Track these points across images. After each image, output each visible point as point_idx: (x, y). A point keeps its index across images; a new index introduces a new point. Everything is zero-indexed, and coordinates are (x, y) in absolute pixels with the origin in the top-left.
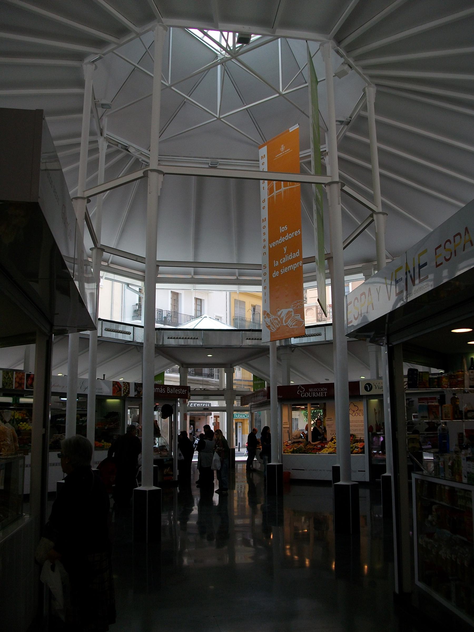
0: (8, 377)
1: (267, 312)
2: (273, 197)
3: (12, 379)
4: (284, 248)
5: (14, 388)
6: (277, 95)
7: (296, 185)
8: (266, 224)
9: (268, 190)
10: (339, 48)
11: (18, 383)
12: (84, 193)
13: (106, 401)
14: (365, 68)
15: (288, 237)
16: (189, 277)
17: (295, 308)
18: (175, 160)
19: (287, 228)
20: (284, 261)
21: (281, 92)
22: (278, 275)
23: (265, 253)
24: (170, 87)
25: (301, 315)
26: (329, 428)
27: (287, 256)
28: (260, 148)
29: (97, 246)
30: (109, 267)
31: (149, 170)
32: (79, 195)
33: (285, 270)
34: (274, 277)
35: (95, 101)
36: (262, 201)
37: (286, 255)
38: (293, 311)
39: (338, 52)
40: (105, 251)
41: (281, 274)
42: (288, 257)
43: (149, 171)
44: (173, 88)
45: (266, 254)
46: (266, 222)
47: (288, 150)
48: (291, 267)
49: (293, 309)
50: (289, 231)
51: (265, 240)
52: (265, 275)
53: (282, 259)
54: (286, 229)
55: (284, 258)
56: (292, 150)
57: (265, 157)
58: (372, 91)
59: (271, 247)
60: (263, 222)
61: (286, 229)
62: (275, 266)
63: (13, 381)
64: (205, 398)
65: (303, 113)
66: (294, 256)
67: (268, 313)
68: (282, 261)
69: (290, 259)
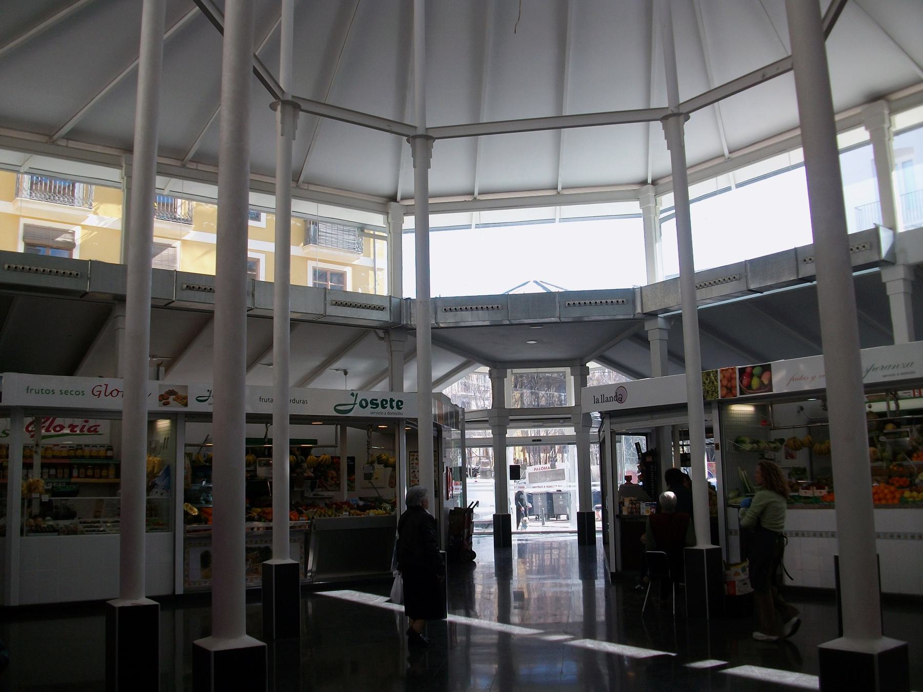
0: (708, 381)
3: (715, 383)
5: (720, 398)
11: (726, 387)
13: (727, 410)
26: (166, 448)
52: (364, 405)
63: (717, 385)
64: (910, 369)
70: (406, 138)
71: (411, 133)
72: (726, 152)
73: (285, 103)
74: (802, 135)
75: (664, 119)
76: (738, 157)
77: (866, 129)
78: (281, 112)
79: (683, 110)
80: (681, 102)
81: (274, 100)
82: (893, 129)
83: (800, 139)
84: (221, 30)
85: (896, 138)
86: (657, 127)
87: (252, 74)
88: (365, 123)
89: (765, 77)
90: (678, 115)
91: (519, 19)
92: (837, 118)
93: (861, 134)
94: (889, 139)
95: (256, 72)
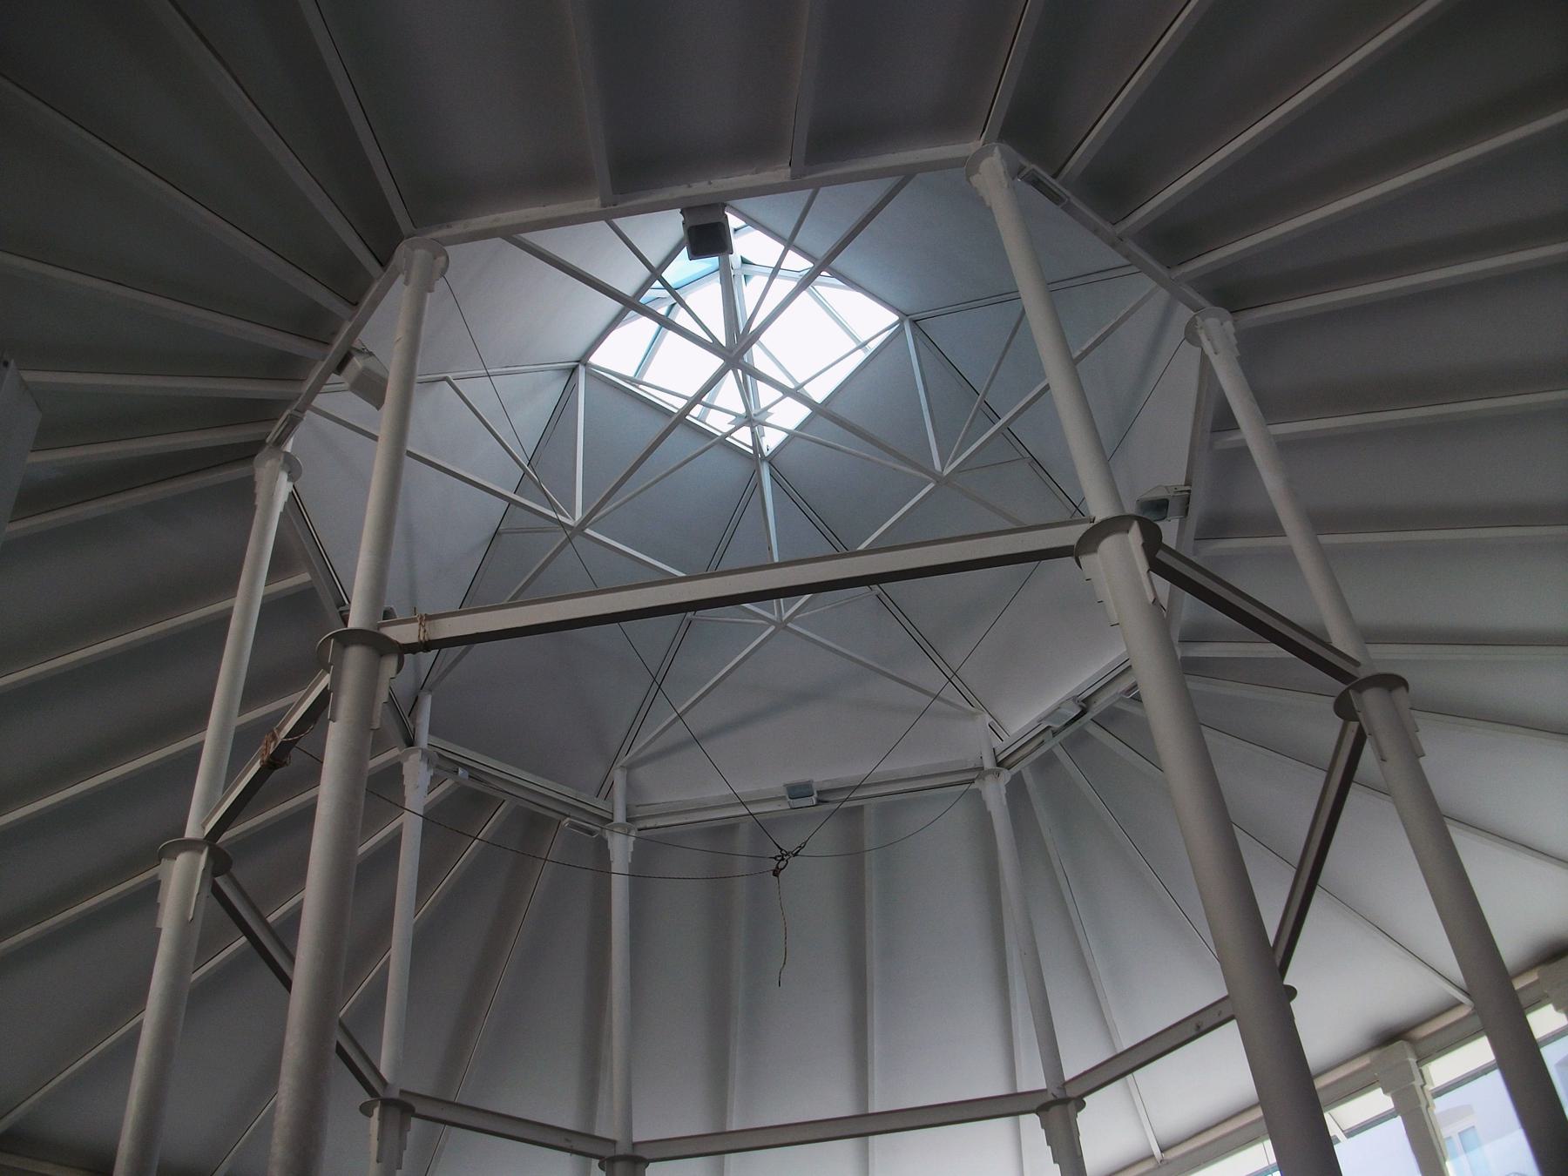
44: (588, 531)
70: (598, 1161)
71: (608, 1152)
72: (1156, 1151)
73: (387, 1103)
74: (1267, 1116)
75: (1041, 1110)
76: (1177, 1158)
77: (1385, 1092)
78: (379, 1119)
79: (1072, 1092)
80: (1067, 1078)
81: (369, 1099)
82: (1429, 1087)
83: (1263, 1125)
84: (287, 983)
85: (1437, 1101)
86: (1031, 1123)
87: (334, 1057)
88: (530, 1138)
89: (1203, 1028)
90: (1064, 1101)
91: (785, 963)
92: (1319, 1083)
93: (1377, 1101)
94: (1428, 1106)
95: (340, 1051)
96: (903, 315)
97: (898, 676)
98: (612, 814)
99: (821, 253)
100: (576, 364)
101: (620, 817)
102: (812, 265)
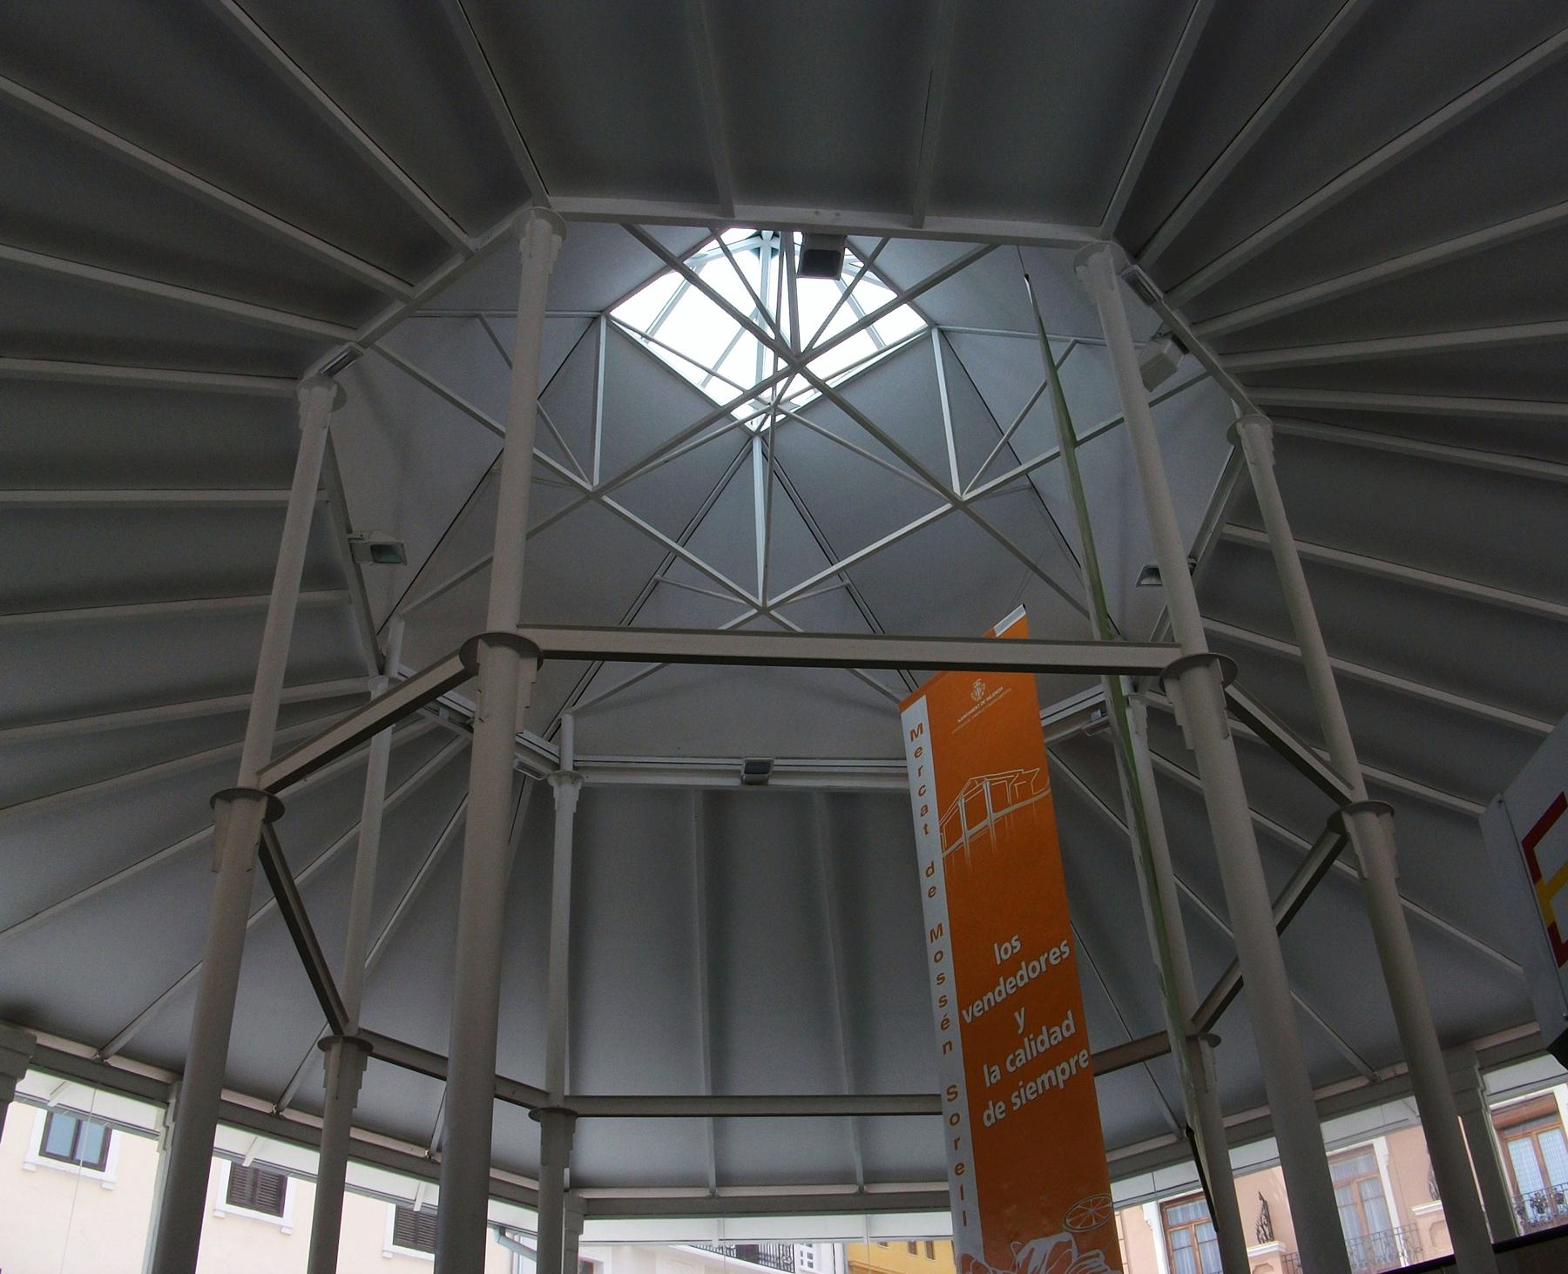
1: (973, 1258)
2: (960, 852)
4: (1016, 1014)
6: (948, 506)
7: (1035, 795)
8: (945, 943)
9: (941, 831)
10: (1136, 267)
12: (259, 779)
14: (1232, 343)
15: (1027, 973)
16: (702, 1193)
17: (1078, 1227)
18: (629, 765)
19: (1018, 944)
20: (1020, 1060)
21: (959, 494)
22: (1004, 1115)
23: (948, 1047)
24: (596, 495)
25: (1104, 1253)
27: (1030, 1040)
28: (905, 705)
29: (342, 1033)
30: (433, 1163)
31: (480, 637)
32: (243, 782)
33: (1029, 1092)
34: (988, 1124)
35: (350, 536)
36: (922, 873)
37: (1026, 1040)
38: (1073, 1241)
39: (1135, 283)
40: (374, 1051)
41: (1015, 1108)
42: (1033, 1043)
43: (480, 641)
44: (606, 499)
45: (953, 1047)
46: (923, 735)
47: (996, 692)
48: (1050, 1077)
49: (1072, 1233)
50: (1031, 952)
51: (956, 1093)
52: (929, 873)
53: (1011, 1057)
54: (1017, 949)
55: (1020, 1051)
56: (1010, 690)
57: (941, 934)
58: (1259, 436)
59: (968, 1020)
60: (932, 941)
61: (1016, 1097)
62: (988, 1085)
65: (1035, 569)
66: (1055, 1038)
67: (979, 1261)
68: (1013, 1063)
69: (1042, 1049)
70: (529, 1110)
96: (932, 323)
97: (694, 569)
98: (560, 759)
99: (907, 284)
100: (599, 314)
101: (568, 766)
102: (895, 296)
